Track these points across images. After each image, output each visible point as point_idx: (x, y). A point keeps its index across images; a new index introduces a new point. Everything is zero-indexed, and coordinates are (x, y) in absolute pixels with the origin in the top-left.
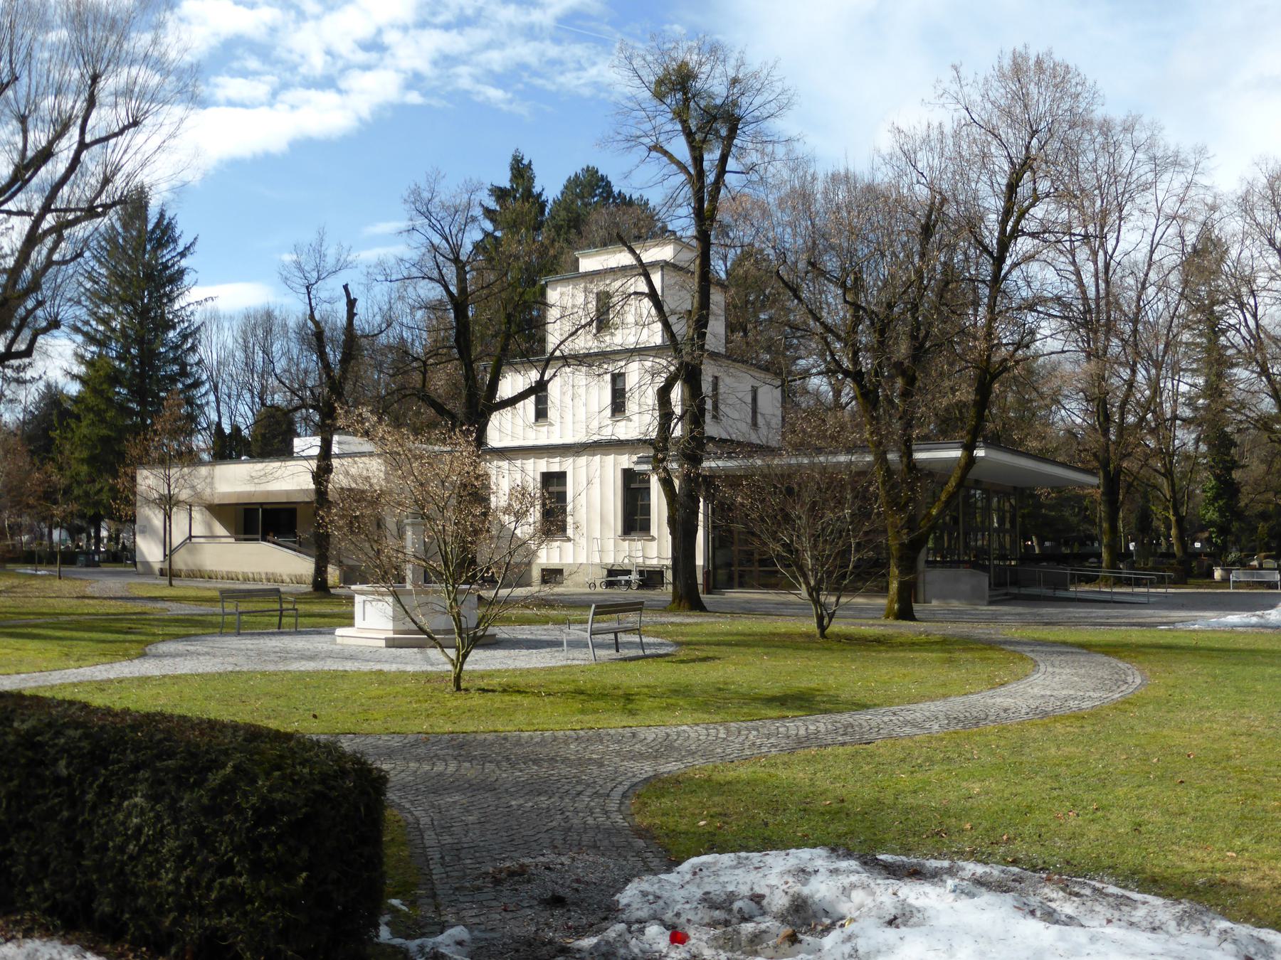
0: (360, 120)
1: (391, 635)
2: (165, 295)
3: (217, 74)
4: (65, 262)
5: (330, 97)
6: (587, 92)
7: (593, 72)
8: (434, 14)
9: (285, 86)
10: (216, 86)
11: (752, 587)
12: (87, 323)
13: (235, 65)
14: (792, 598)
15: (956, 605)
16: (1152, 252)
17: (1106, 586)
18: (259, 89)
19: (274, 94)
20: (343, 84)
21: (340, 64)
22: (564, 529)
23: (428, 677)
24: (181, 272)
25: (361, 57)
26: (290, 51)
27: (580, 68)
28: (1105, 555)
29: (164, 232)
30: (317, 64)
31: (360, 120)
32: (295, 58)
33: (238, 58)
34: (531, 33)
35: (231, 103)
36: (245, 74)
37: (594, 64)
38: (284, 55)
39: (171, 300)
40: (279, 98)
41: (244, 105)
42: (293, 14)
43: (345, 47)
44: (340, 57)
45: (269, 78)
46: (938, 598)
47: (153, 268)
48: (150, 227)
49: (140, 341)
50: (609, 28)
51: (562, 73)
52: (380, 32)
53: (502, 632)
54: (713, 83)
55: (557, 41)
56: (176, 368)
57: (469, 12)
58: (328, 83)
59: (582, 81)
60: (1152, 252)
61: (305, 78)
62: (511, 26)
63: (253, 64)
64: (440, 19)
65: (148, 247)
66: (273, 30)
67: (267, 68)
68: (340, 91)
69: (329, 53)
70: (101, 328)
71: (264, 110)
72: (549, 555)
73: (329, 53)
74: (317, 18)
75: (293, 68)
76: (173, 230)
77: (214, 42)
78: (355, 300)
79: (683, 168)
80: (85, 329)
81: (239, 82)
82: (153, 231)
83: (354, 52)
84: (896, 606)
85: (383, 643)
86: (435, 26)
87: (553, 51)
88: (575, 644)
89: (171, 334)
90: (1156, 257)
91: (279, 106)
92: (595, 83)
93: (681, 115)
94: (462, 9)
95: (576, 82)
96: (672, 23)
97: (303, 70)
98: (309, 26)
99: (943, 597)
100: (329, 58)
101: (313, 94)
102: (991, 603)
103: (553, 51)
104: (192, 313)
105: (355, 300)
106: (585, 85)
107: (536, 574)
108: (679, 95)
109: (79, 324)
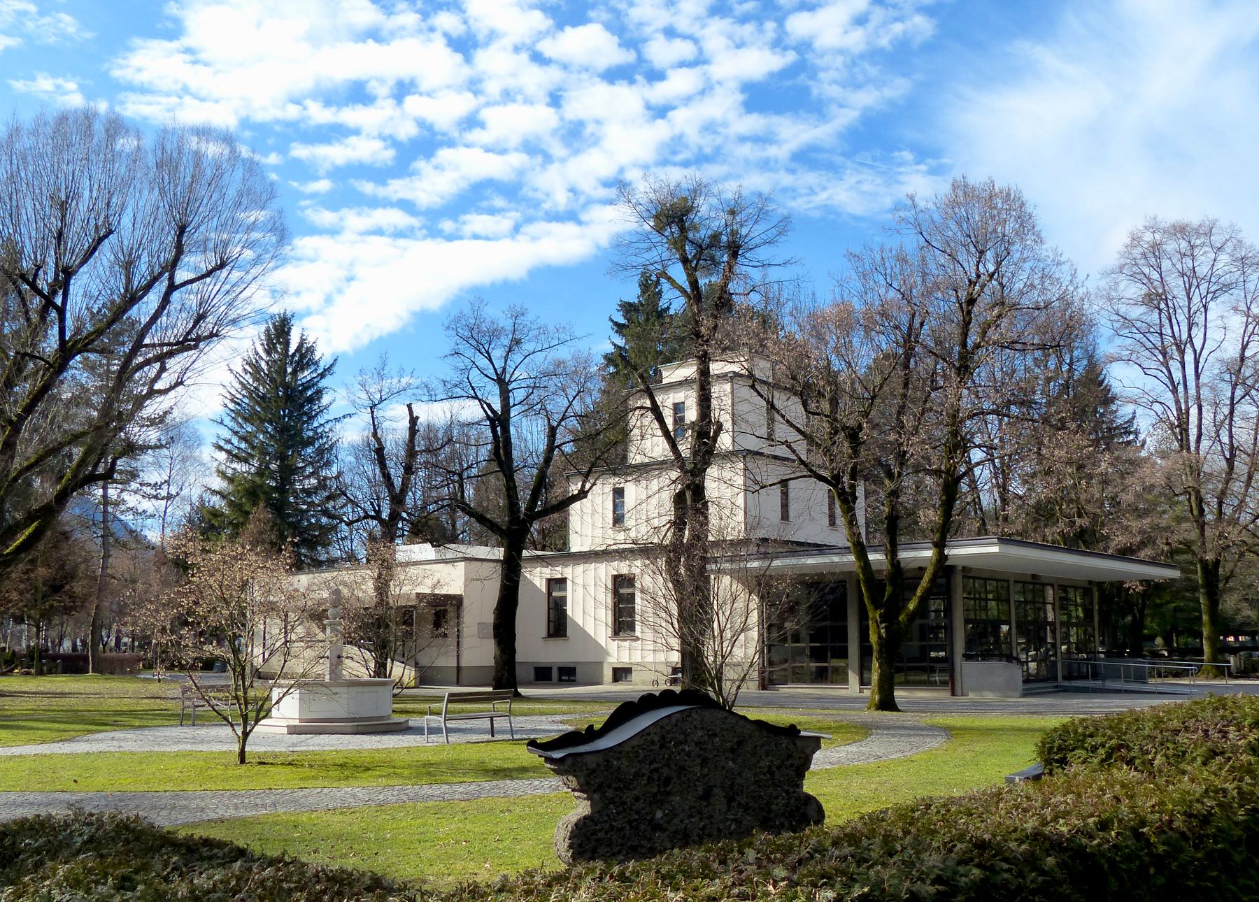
0: (598, 247)
1: (297, 723)
2: (306, 413)
3: (465, 213)
4: (165, 392)
5: (570, 228)
6: (816, 214)
7: (823, 196)
8: (674, 153)
9: (529, 220)
10: (464, 223)
11: (805, 682)
12: (229, 441)
13: (484, 204)
14: (843, 693)
15: (990, 696)
16: (1244, 348)
17: (1207, 678)
18: (504, 223)
19: (517, 229)
20: (584, 217)
21: (582, 199)
22: (633, 629)
23: (209, 758)
24: (319, 393)
25: (603, 193)
26: (536, 190)
27: (812, 192)
28: (1206, 648)
29: (303, 356)
30: (561, 199)
31: (598, 247)
32: (539, 195)
33: (487, 199)
34: (766, 165)
35: (476, 237)
36: (492, 211)
37: (824, 189)
38: (531, 194)
39: (311, 418)
40: (522, 230)
41: (488, 239)
42: (539, 159)
43: (588, 186)
44: (583, 193)
45: (514, 214)
46: (973, 690)
47: (293, 390)
48: (292, 350)
49: (282, 457)
50: (842, 158)
51: (794, 198)
52: (622, 170)
53: (414, 721)
54: (709, 217)
55: (791, 171)
56: (314, 481)
57: (708, 150)
58: (571, 216)
59: (812, 205)
60: (1244, 348)
61: (547, 213)
62: (747, 161)
63: (499, 202)
64: (680, 157)
65: (289, 370)
66: (521, 173)
67: (513, 205)
68: (579, 223)
69: (573, 190)
70: (243, 445)
71: (507, 243)
72: (618, 653)
73: (573, 190)
74: (563, 160)
75: (536, 204)
76: (312, 353)
77: (464, 185)
78: (417, 418)
79: (683, 291)
80: (228, 447)
81: (485, 218)
82: (294, 355)
83: (595, 189)
84: (877, 697)
85: (285, 730)
86: (675, 164)
87: (786, 180)
88: (432, 731)
89: (310, 450)
90: (1248, 353)
91: (520, 237)
92: (825, 206)
93: (678, 244)
94: (701, 149)
95: (806, 206)
96: (900, 150)
97: (546, 206)
98: (554, 168)
99: (978, 689)
100: (571, 194)
101: (555, 227)
102: (1024, 695)
103: (786, 180)
104: (331, 430)
105: (417, 418)
106: (816, 208)
107: (608, 674)
108: (675, 229)
109: (222, 443)
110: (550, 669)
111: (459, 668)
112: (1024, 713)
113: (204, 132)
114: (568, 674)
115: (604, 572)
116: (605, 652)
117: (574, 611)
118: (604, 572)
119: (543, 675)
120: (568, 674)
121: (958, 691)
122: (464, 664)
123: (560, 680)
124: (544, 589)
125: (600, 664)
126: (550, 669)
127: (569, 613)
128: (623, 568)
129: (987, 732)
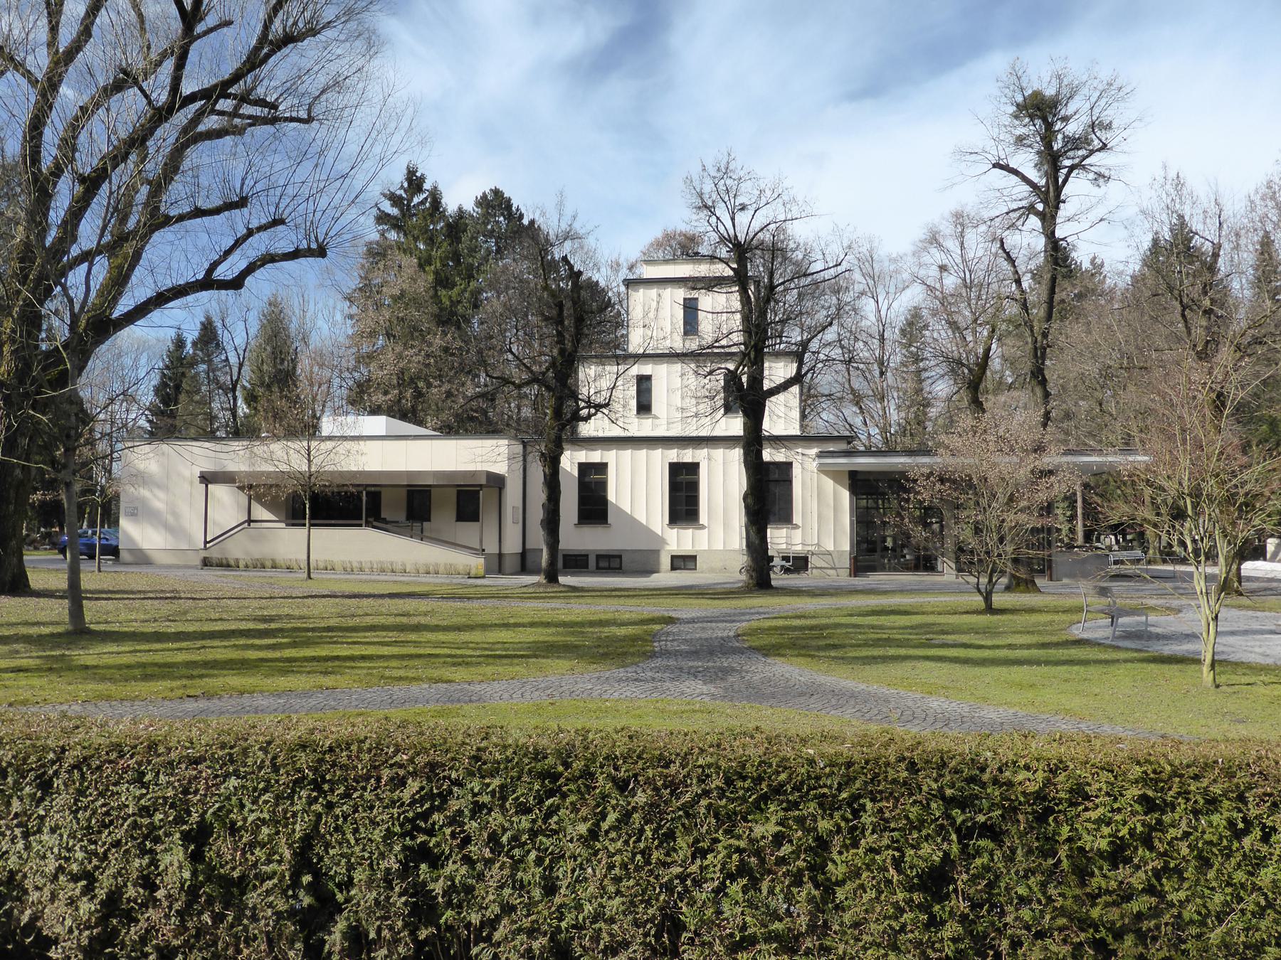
72: (679, 540)
107: (665, 562)
110: (587, 556)
111: (500, 555)
112: (1233, 607)
113: (177, 140)
114: (610, 563)
115: (661, 459)
116: (663, 541)
117: (618, 493)
118: (661, 459)
119: (577, 562)
120: (610, 563)
121: (1054, 577)
122: (505, 551)
123: (598, 568)
124: (576, 474)
125: (656, 553)
126: (587, 556)
127: (611, 497)
128: (688, 456)
129: (786, 618)
